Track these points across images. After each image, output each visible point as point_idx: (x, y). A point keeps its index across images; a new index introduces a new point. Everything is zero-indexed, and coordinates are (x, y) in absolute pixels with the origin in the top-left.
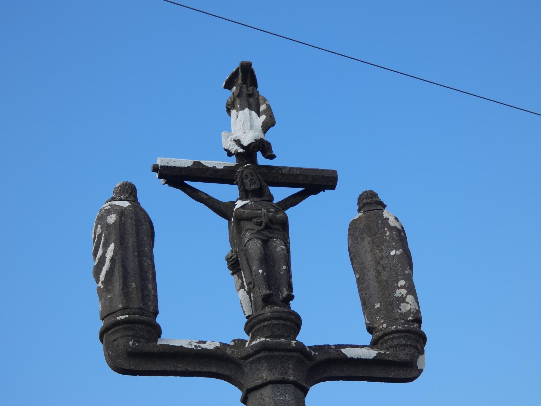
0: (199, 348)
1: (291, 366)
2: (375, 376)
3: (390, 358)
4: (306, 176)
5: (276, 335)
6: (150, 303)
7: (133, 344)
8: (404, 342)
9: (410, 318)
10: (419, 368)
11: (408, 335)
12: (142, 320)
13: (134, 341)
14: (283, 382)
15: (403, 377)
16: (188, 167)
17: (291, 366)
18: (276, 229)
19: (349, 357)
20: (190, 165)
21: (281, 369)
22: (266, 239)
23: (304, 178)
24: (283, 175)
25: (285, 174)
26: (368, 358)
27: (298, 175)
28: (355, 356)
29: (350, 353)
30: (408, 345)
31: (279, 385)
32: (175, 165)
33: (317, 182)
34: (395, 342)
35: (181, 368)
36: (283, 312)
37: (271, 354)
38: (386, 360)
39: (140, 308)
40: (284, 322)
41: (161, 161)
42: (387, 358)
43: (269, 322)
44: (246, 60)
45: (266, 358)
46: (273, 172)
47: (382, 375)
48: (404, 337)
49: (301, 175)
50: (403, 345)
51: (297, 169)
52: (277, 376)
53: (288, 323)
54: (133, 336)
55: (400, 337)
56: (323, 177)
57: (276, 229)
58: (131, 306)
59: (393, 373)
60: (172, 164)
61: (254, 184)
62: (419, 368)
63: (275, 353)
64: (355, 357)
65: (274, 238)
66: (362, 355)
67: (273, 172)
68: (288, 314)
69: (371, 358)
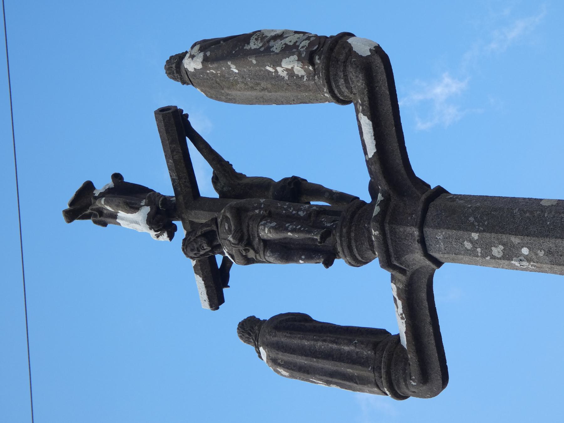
0: (404, 316)
1: (401, 229)
2: (391, 111)
3: (366, 99)
4: (172, 152)
5: (370, 246)
6: (365, 353)
7: (414, 381)
8: (342, 81)
9: (311, 68)
10: (370, 54)
11: (332, 77)
12: (386, 375)
13: (411, 379)
14: (422, 241)
15: (385, 77)
16: (203, 280)
17: (401, 229)
18: (248, 231)
19: (375, 150)
20: (201, 279)
21: (408, 240)
22: (262, 244)
23: (175, 153)
24: (180, 178)
25: (178, 176)
26: (372, 128)
27: (174, 161)
28: (372, 143)
29: (372, 150)
30: (344, 76)
31: (427, 244)
32: (205, 293)
33: (175, 127)
34: (344, 89)
35: (429, 329)
36: (342, 245)
37: (393, 254)
38: (370, 104)
39: (374, 371)
40: (353, 241)
41: (205, 305)
42: (366, 103)
43: (357, 255)
44: (62, 218)
45: (398, 259)
46: (179, 189)
47: (389, 102)
48: (336, 82)
49: (173, 157)
50: (346, 81)
51: (168, 162)
52: (417, 246)
53: (353, 235)
54: (405, 381)
55: (338, 87)
56: (167, 132)
57: (248, 231)
58: (374, 380)
59: (383, 88)
60: (205, 297)
61: (203, 247)
62: (370, 54)
63: (391, 250)
64: (374, 142)
65: (259, 236)
66: (370, 135)
67: (179, 189)
68: (343, 239)
69: (371, 123)
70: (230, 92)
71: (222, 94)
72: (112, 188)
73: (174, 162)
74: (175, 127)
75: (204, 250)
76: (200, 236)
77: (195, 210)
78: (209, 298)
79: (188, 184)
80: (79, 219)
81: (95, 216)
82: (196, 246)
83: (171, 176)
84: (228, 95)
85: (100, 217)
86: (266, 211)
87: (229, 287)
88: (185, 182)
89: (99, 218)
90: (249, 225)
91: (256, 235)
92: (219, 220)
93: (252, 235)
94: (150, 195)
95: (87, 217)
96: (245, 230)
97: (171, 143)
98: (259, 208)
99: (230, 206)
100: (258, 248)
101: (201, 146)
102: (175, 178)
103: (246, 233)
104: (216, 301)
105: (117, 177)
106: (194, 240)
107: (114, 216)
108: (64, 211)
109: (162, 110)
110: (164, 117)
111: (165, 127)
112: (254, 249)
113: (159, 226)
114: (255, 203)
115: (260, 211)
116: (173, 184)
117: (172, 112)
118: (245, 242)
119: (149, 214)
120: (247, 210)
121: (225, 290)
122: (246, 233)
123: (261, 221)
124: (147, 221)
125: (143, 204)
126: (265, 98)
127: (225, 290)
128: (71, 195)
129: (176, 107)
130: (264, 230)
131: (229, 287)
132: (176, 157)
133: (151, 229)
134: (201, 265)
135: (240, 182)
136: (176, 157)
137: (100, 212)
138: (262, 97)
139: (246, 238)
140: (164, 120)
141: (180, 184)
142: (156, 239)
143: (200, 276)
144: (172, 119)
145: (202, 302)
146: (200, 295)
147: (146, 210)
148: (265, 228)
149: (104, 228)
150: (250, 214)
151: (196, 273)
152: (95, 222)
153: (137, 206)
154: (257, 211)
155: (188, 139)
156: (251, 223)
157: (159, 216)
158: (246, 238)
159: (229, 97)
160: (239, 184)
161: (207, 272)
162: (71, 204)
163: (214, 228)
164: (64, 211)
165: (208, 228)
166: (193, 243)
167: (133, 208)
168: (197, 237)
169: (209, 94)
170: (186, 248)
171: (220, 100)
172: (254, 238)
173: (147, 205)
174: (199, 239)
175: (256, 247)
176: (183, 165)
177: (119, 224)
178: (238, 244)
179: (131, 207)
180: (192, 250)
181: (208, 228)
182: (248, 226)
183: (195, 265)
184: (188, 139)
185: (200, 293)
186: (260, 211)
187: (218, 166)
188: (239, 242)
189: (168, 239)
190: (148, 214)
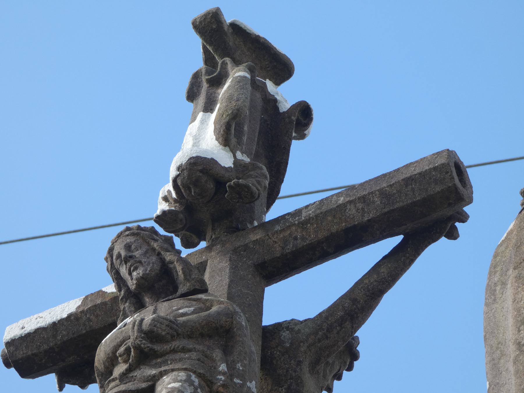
4: (363, 199)
16: (70, 316)
18: (174, 351)
22: (144, 385)
23: (360, 206)
25: (308, 220)
27: (342, 207)
32: (39, 325)
33: (424, 206)
46: (278, 228)
49: (350, 202)
56: (409, 181)
61: (136, 269)
65: (162, 374)
67: (278, 228)
70: (509, 286)
71: (504, 273)
72: (277, 108)
73: (339, 206)
74: (424, 206)
75: (130, 274)
76: (163, 261)
77: (231, 268)
78: (28, 335)
79: (290, 247)
80: (204, 47)
81: (208, 73)
82: (137, 254)
83: (307, 207)
84: (504, 284)
85: (209, 81)
86: (223, 386)
87: (61, 388)
88: (296, 238)
89: (204, 78)
90: (190, 350)
91: (163, 369)
92: (200, 296)
93: (167, 361)
94: (261, 169)
95: (209, 59)
96: (175, 344)
97: (382, 193)
98: (232, 373)
99: (235, 313)
100: (133, 379)
101: (383, 269)
102: (304, 214)
103: (166, 347)
104: (20, 354)
105: (303, 114)
106: (154, 249)
107: (208, 108)
108: (218, 9)
109: (460, 170)
110: (441, 169)
111: (420, 174)
112: (129, 370)
113: (187, 188)
114: (244, 366)
115: (224, 374)
116: (288, 214)
117: (456, 188)
118: (146, 345)
119: (213, 162)
120: (227, 351)
121: (51, 379)
122: (166, 347)
123: (199, 376)
124: (198, 158)
125: (239, 155)
126: (502, 361)
127: (51, 379)
128: (256, 26)
129: (470, 201)
130: (175, 381)
131: (61, 388)
132: (351, 210)
133: (178, 169)
134: (104, 304)
135: (306, 367)
136: (351, 210)
137: (217, 82)
138: (502, 355)
139: (157, 347)
140: (435, 169)
141: (289, 227)
142: (161, 195)
143: (79, 307)
144: (438, 189)
145: (21, 323)
146: (36, 316)
147: (226, 160)
148: (180, 381)
149: (185, 98)
150: (217, 354)
151: (87, 297)
152: (196, 76)
153: (233, 141)
154: (223, 367)
155: (398, 239)
156: (194, 355)
157: (211, 186)
158: (157, 347)
159: (498, 288)
160: (299, 363)
161: (89, 320)
162: (236, 27)
163: (182, 289)
164: (218, 9)
165: (180, 273)
166: (145, 248)
167: (228, 134)
168: (159, 254)
169: (503, 248)
170: (133, 234)
171: (492, 273)
172: (155, 366)
173: (236, 162)
174: (154, 259)
175: (137, 373)
176: (334, 229)
177: (194, 119)
178: (140, 330)
179: (228, 126)
180: (128, 247)
181: (180, 273)
182: (184, 350)
183: (104, 293)
184: (398, 239)
185: (41, 315)
186: (224, 374)
187: (340, 313)
188: (145, 333)
189: (158, 212)
190: (212, 159)
